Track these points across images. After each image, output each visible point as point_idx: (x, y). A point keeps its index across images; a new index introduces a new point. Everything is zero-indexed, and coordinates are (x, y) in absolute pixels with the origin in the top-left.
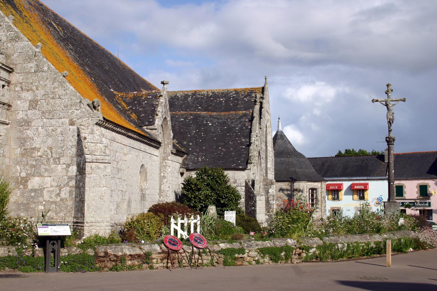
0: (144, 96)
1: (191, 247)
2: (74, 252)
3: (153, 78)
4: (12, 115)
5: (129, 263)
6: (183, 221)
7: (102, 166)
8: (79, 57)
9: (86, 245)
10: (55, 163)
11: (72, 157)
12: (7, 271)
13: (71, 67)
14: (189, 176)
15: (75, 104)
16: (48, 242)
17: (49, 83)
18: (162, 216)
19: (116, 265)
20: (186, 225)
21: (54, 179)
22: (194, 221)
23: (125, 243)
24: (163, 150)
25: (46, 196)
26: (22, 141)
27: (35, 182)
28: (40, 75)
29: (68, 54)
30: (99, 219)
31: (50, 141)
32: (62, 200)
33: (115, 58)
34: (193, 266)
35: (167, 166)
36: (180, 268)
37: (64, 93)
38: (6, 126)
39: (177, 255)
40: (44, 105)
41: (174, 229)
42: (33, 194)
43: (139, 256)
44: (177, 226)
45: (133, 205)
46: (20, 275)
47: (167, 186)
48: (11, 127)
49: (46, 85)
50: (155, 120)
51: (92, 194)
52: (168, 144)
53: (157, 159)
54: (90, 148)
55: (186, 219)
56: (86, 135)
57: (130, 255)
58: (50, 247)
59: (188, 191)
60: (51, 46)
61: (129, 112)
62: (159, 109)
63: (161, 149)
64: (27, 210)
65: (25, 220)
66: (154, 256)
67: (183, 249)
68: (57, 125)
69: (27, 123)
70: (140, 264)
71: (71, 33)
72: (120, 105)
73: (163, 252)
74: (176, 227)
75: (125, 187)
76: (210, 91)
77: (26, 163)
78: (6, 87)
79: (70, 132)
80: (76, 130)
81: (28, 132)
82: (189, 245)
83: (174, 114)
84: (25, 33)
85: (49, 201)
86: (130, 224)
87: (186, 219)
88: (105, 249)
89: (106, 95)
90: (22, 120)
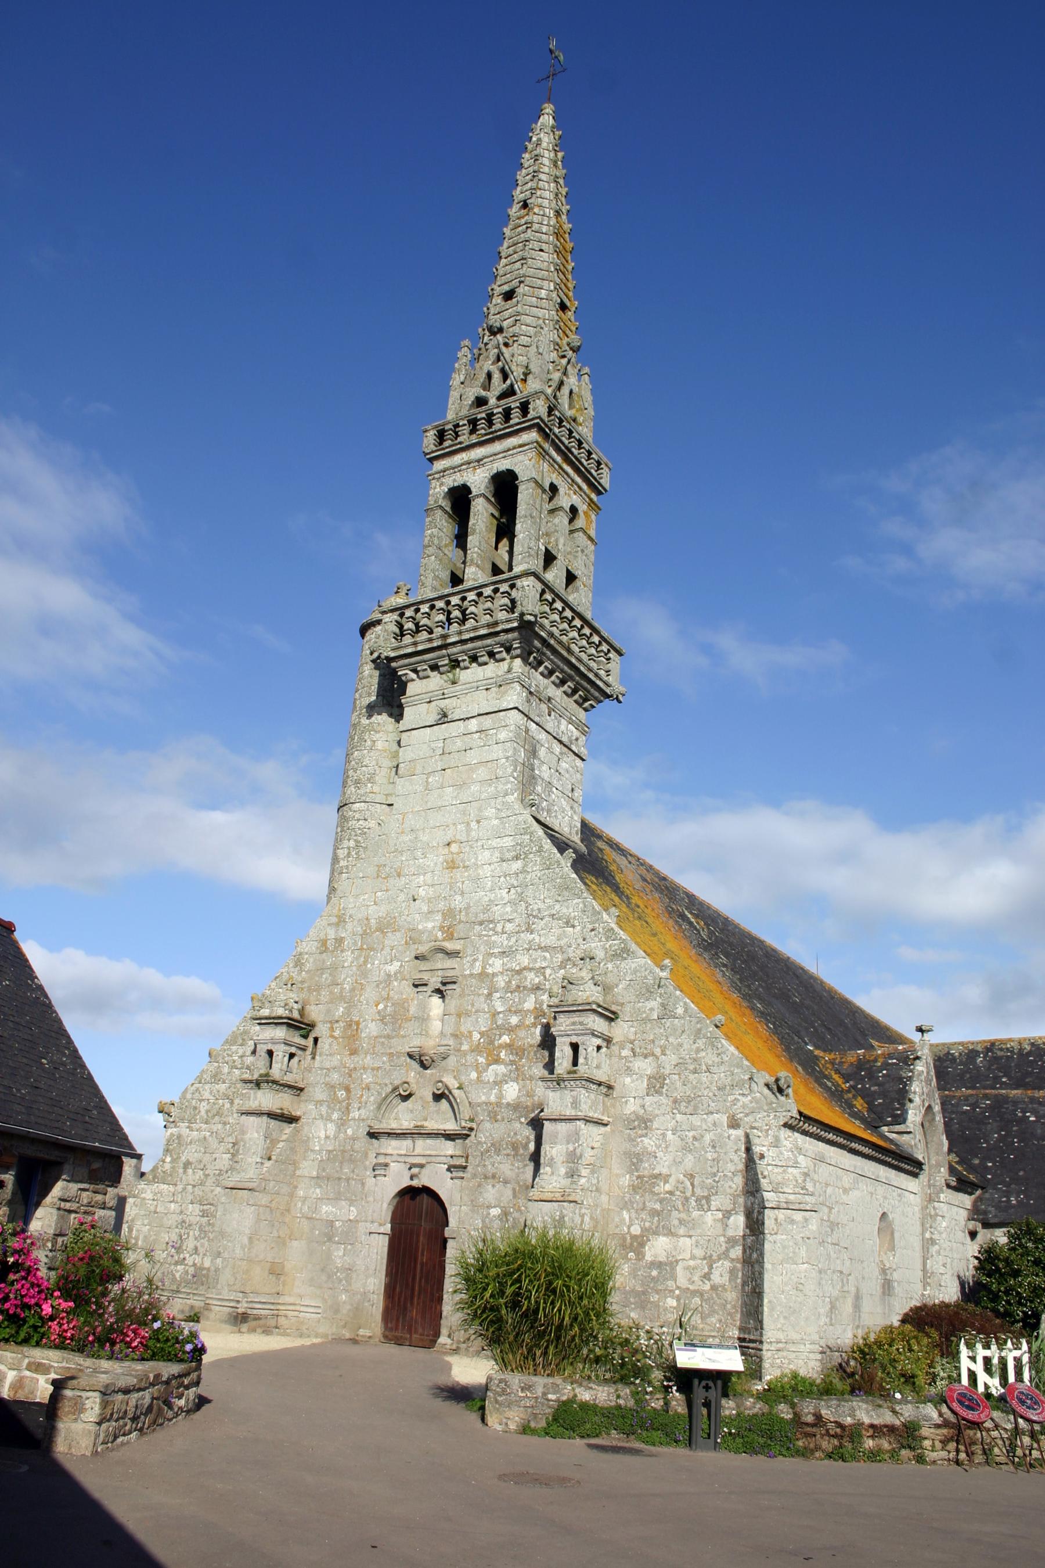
0: (881, 1060)
1: (1012, 1417)
2: (750, 1409)
3: (903, 1025)
4: (613, 1106)
5: (870, 1443)
6: (987, 1353)
7: (798, 1216)
8: (741, 980)
9: (772, 1394)
10: (700, 1208)
11: (734, 1196)
12: (614, 1439)
13: (729, 1006)
14: (992, 1240)
15: (740, 1084)
16: (696, 1382)
17: (686, 1041)
18: (935, 1335)
19: (841, 1446)
20: (995, 1361)
21: (697, 1242)
22: (1016, 1353)
23: (857, 1396)
24: (926, 1180)
25: (682, 1280)
26: (635, 1160)
27: (658, 1247)
28: (668, 1024)
29: (719, 975)
30: (795, 1336)
31: (689, 1161)
32: (714, 1288)
33: (812, 977)
34: (1019, 1464)
35: (937, 1215)
36: (987, 1468)
37: (717, 1060)
38: (603, 1129)
39: (979, 1435)
40: (677, 1086)
41: (969, 1370)
42: (654, 1273)
43: (892, 1429)
44: (972, 1360)
45: (866, 1305)
46: (641, 1451)
47: (941, 1263)
48: (613, 1131)
49: (681, 1045)
50: (907, 1113)
51: (778, 1279)
52: (939, 1165)
53: (915, 1200)
54: (773, 1177)
55: (994, 1347)
56: (764, 1149)
57: (872, 1426)
58: (699, 1394)
59: (989, 1276)
60: (687, 962)
61: (850, 1095)
62: (916, 1087)
63: (923, 1177)
64: (642, 1306)
65: (648, 1332)
66: (925, 1432)
67: (992, 1419)
68: (704, 1127)
69: (643, 1122)
70: (893, 1449)
71: (722, 930)
72: (828, 1079)
73: (946, 1424)
74: (973, 1367)
75: (848, 1263)
76: (1025, 1039)
77: (641, 1206)
78: (604, 1050)
79: (730, 1143)
80: (743, 1139)
81: (646, 1140)
82: (1007, 1413)
83: (947, 1096)
84: (639, 940)
85: (688, 1289)
86: (862, 1351)
87: (994, 1347)
88: (815, 1407)
89: (800, 1059)
90: (633, 1117)
